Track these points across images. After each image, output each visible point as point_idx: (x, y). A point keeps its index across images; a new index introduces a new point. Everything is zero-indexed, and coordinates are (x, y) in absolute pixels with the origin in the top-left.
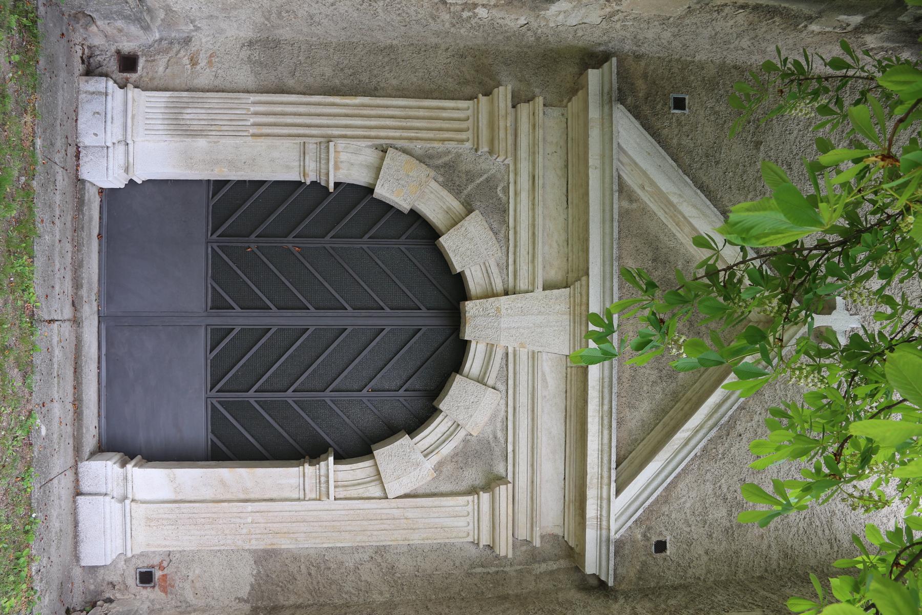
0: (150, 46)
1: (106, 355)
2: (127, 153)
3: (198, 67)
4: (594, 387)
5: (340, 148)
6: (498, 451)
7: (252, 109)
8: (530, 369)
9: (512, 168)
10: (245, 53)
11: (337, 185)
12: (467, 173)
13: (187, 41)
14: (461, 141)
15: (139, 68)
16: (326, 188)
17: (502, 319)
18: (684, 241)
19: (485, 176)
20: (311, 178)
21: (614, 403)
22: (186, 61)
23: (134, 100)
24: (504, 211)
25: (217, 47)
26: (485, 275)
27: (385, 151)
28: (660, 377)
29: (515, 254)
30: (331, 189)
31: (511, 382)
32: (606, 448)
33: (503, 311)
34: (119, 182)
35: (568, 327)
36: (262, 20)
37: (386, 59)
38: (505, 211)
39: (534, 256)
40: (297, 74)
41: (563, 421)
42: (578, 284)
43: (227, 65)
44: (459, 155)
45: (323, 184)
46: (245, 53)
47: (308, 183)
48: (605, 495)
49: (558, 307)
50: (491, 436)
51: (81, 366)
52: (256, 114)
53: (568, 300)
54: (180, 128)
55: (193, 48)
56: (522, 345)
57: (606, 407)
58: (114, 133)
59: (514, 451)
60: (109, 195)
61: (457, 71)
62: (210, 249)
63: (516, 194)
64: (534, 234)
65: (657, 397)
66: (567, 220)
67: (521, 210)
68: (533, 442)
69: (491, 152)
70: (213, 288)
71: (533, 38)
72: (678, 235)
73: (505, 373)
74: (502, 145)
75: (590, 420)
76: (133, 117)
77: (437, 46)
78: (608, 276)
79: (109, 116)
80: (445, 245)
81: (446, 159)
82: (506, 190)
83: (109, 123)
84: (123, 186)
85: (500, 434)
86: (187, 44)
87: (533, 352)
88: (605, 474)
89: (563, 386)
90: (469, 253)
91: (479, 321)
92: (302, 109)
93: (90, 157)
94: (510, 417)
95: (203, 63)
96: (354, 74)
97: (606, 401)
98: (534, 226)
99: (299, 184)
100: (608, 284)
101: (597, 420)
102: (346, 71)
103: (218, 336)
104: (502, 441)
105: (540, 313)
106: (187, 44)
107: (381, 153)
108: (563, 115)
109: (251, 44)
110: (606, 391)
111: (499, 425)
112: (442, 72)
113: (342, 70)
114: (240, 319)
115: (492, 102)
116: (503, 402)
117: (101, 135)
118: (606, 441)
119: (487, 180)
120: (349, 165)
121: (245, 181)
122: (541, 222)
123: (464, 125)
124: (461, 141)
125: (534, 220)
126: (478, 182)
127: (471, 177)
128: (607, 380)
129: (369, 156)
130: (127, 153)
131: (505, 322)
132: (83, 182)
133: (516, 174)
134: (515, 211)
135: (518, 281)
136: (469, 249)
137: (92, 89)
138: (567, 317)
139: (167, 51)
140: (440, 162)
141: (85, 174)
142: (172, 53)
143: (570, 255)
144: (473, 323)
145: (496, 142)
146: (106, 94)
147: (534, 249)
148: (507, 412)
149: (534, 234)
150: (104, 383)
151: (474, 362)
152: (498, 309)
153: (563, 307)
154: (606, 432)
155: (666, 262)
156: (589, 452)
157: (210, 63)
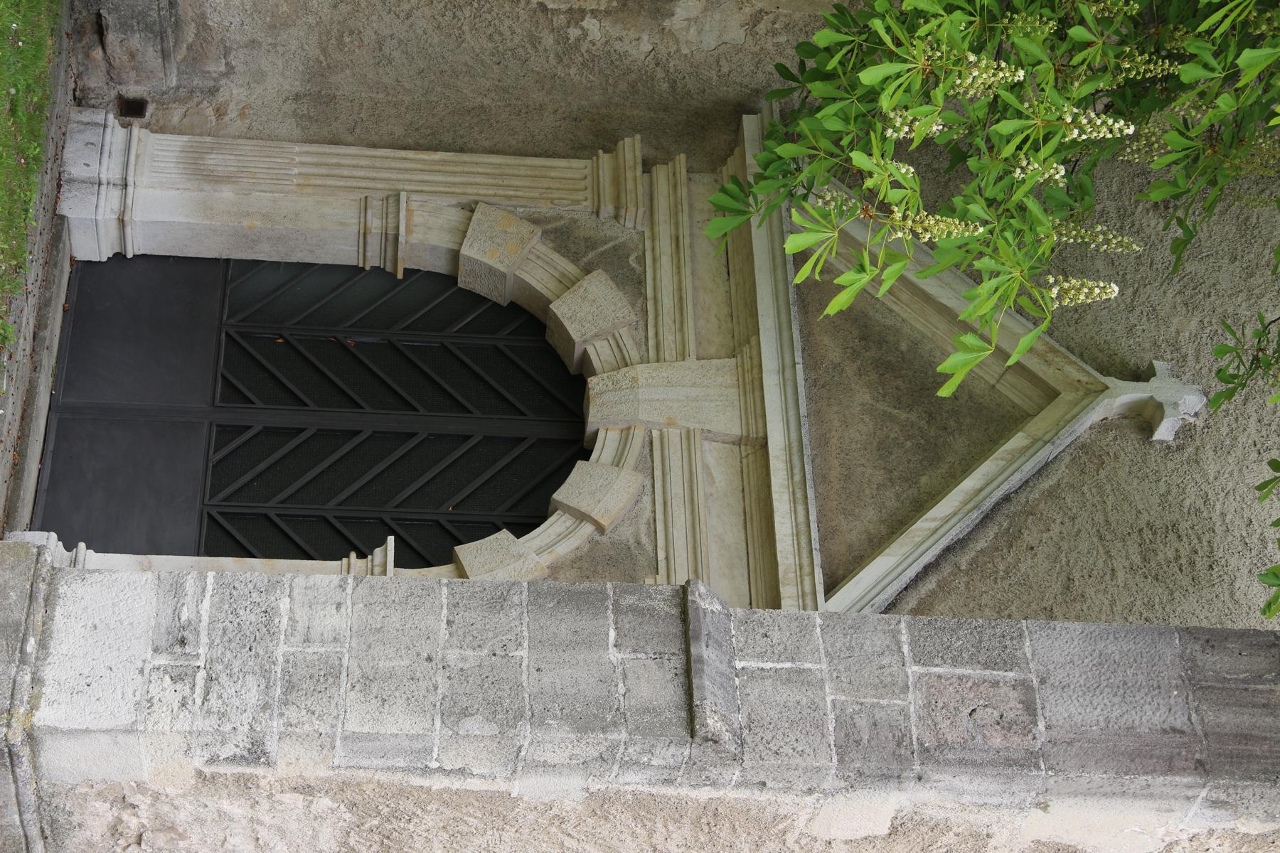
0: (164, 93)
1: (54, 452)
2: (124, 197)
3: (226, 118)
4: (777, 457)
5: (414, 206)
6: (642, 561)
7: (297, 159)
8: (685, 454)
9: (647, 234)
10: (289, 107)
11: (408, 272)
12: (586, 239)
13: (213, 91)
14: (577, 202)
15: (148, 114)
16: (394, 275)
17: (640, 390)
18: (905, 316)
19: (611, 244)
20: (373, 260)
21: (808, 468)
22: (210, 112)
23: (139, 139)
24: (640, 283)
25: (252, 99)
26: (616, 350)
27: (470, 208)
28: (890, 480)
29: (656, 326)
30: (400, 276)
31: (658, 473)
32: (803, 528)
33: (641, 381)
34: (102, 252)
35: (737, 403)
36: (317, 52)
37: (475, 120)
38: (641, 282)
39: (682, 323)
40: (358, 131)
41: (741, 527)
42: (746, 349)
43: (264, 119)
44: (575, 221)
45: (389, 268)
46: (289, 107)
47: (368, 268)
48: (808, 588)
49: (721, 379)
50: (631, 541)
51: (31, 415)
52: (303, 164)
53: (734, 371)
54: (197, 171)
55: (222, 97)
56: (671, 423)
57: (797, 478)
58: (110, 170)
59: (667, 558)
60: (84, 269)
61: (570, 136)
62: (223, 335)
63: (654, 260)
64: (681, 298)
65: (888, 504)
66: (728, 292)
67: (663, 278)
68: (696, 559)
69: (616, 217)
70: (224, 377)
71: (666, 85)
72: (894, 307)
73: (649, 464)
74: (631, 196)
75: (775, 496)
76: (137, 156)
77: (542, 107)
78: (785, 325)
79: (107, 148)
80: (558, 314)
81: (558, 224)
82: (641, 260)
83: (106, 155)
84: (104, 259)
85: (645, 540)
86: (213, 94)
87: (688, 432)
88: (806, 561)
89: (737, 483)
90: (590, 317)
91: (606, 397)
92: (363, 162)
93: (74, 193)
94: (659, 516)
95: (233, 113)
96: (433, 134)
97: (797, 471)
98: (680, 290)
99: (356, 270)
100: (786, 334)
101: (786, 497)
102: (422, 131)
103: (226, 432)
104: (650, 548)
105: (694, 385)
106: (213, 94)
107: (469, 213)
108: (716, 181)
109: (297, 97)
110: (796, 459)
111: (643, 529)
112: (550, 136)
113: (417, 129)
114: (261, 417)
115: (617, 157)
116: (648, 483)
117: (95, 166)
118: (801, 518)
119: (615, 248)
120: (425, 236)
121: (278, 263)
122: (689, 285)
123: (581, 185)
124: (577, 202)
125: (680, 282)
126: (601, 249)
127: (591, 244)
128: (795, 445)
129: (453, 216)
130: (124, 197)
131: (643, 394)
132: (62, 218)
133: (653, 240)
134: (654, 279)
135: (661, 353)
136: (588, 314)
137: (86, 120)
138: (735, 391)
139: (183, 101)
140: (549, 227)
141: (65, 208)
142: (192, 104)
143: (736, 329)
144: (598, 401)
145: (623, 195)
146: (105, 126)
147: (682, 315)
148: (654, 512)
149: (681, 298)
150: (45, 485)
151: (605, 448)
152: (635, 380)
153: (730, 379)
154: (800, 508)
155: (881, 342)
156: (780, 546)
157: (242, 115)
